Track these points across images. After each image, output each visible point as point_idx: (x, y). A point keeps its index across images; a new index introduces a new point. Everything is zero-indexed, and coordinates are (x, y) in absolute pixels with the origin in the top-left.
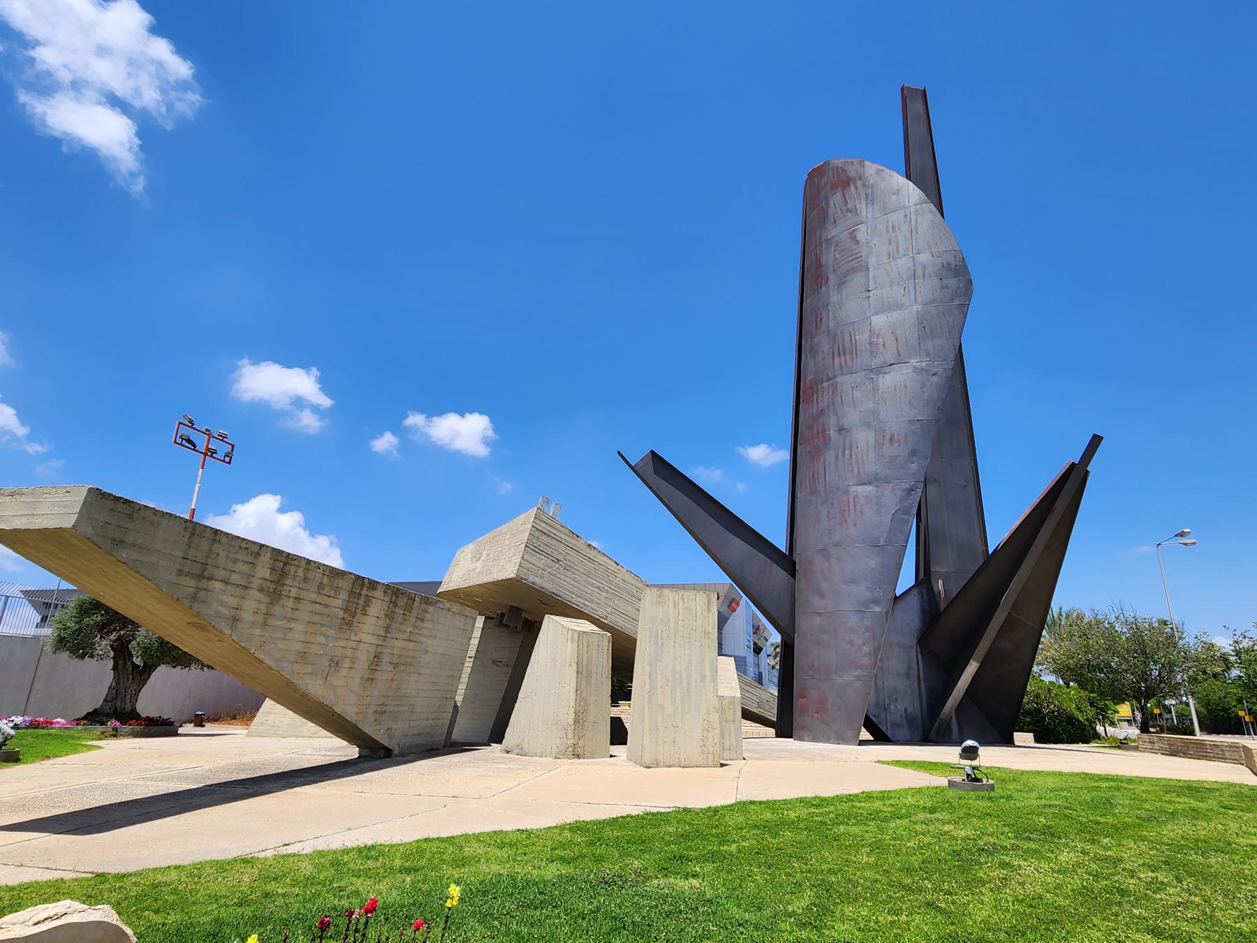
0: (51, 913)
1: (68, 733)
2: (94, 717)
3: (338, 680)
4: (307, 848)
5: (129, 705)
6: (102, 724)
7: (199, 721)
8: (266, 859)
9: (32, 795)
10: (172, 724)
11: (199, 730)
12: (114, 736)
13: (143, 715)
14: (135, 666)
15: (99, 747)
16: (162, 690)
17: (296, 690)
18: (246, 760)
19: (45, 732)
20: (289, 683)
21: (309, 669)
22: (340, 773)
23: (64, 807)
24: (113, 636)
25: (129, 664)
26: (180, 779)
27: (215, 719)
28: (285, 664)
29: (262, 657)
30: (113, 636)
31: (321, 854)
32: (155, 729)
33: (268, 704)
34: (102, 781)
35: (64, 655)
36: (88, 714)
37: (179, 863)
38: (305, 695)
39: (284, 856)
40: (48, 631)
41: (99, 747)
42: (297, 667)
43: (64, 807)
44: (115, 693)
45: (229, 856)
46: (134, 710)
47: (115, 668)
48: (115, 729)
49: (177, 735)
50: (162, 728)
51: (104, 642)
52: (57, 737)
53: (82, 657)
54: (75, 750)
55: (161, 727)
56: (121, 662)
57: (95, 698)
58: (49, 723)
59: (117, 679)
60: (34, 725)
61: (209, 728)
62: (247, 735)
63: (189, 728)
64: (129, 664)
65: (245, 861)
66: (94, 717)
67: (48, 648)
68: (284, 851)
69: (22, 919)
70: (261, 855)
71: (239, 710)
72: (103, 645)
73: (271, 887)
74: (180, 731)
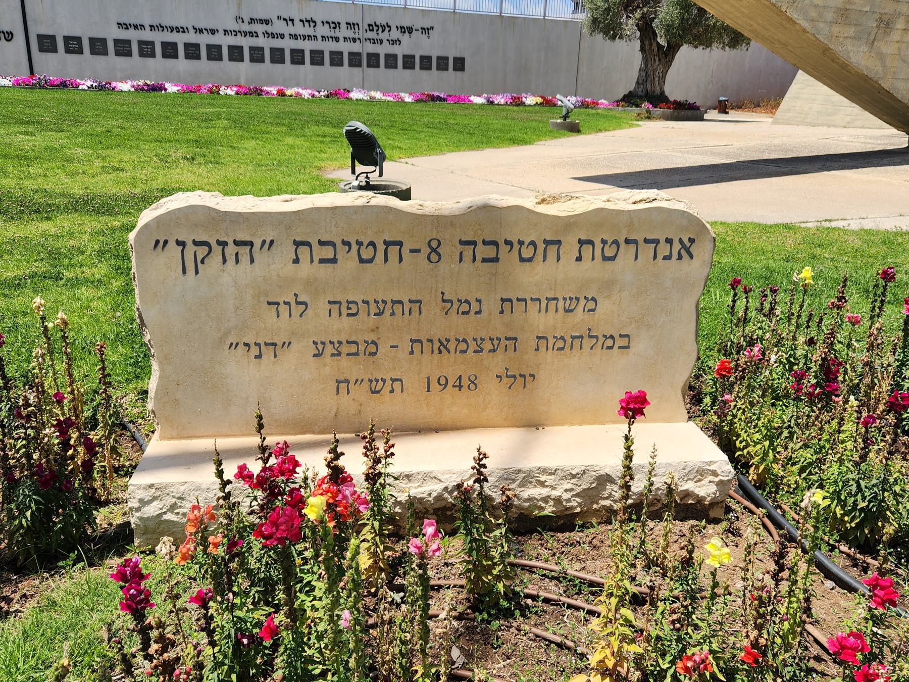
0: (645, 197)
1: (611, 113)
2: (630, 99)
3: (888, 47)
4: (854, 226)
5: (658, 88)
6: (637, 106)
7: (723, 108)
8: (809, 229)
9: (595, 157)
10: (698, 108)
11: (723, 117)
12: (649, 118)
13: (672, 99)
14: (660, 47)
15: (639, 126)
16: (689, 70)
17: (834, 58)
18: (776, 142)
19: (594, 111)
20: (826, 50)
21: (851, 31)
22: (885, 161)
23: (621, 168)
24: (638, 14)
25: (654, 45)
26: (713, 154)
27: (739, 107)
28: (822, 25)
29: (795, 16)
30: (638, 14)
31: (869, 232)
32: (683, 113)
33: (800, 72)
34: (646, 151)
35: (599, 37)
36: (625, 96)
37: (723, 220)
38: (845, 66)
39: (828, 228)
40: (583, 17)
41: (639, 126)
42: (836, 29)
43: (621, 168)
44: (646, 75)
45: (770, 222)
46: (663, 93)
47: (643, 49)
48: (648, 112)
49: (702, 119)
50: (690, 113)
51: (631, 21)
52: (605, 117)
53: (613, 38)
54: (619, 127)
55: (687, 111)
56: (647, 43)
57: (628, 82)
58: (595, 104)
59: (645, 60)
60: (584, 105)
61: (733, 115)
62: (774, 123)
63: (713, 114)
64: (654, 45)
65: (787, 227)
66: (630, 99)
67: (585, 31)
68: (827, 224)
69: (624, 197)
70: (803, 225)
71: (765, 96)
72: (630, 25)
73: (818, 251)
74: (706, 116)
